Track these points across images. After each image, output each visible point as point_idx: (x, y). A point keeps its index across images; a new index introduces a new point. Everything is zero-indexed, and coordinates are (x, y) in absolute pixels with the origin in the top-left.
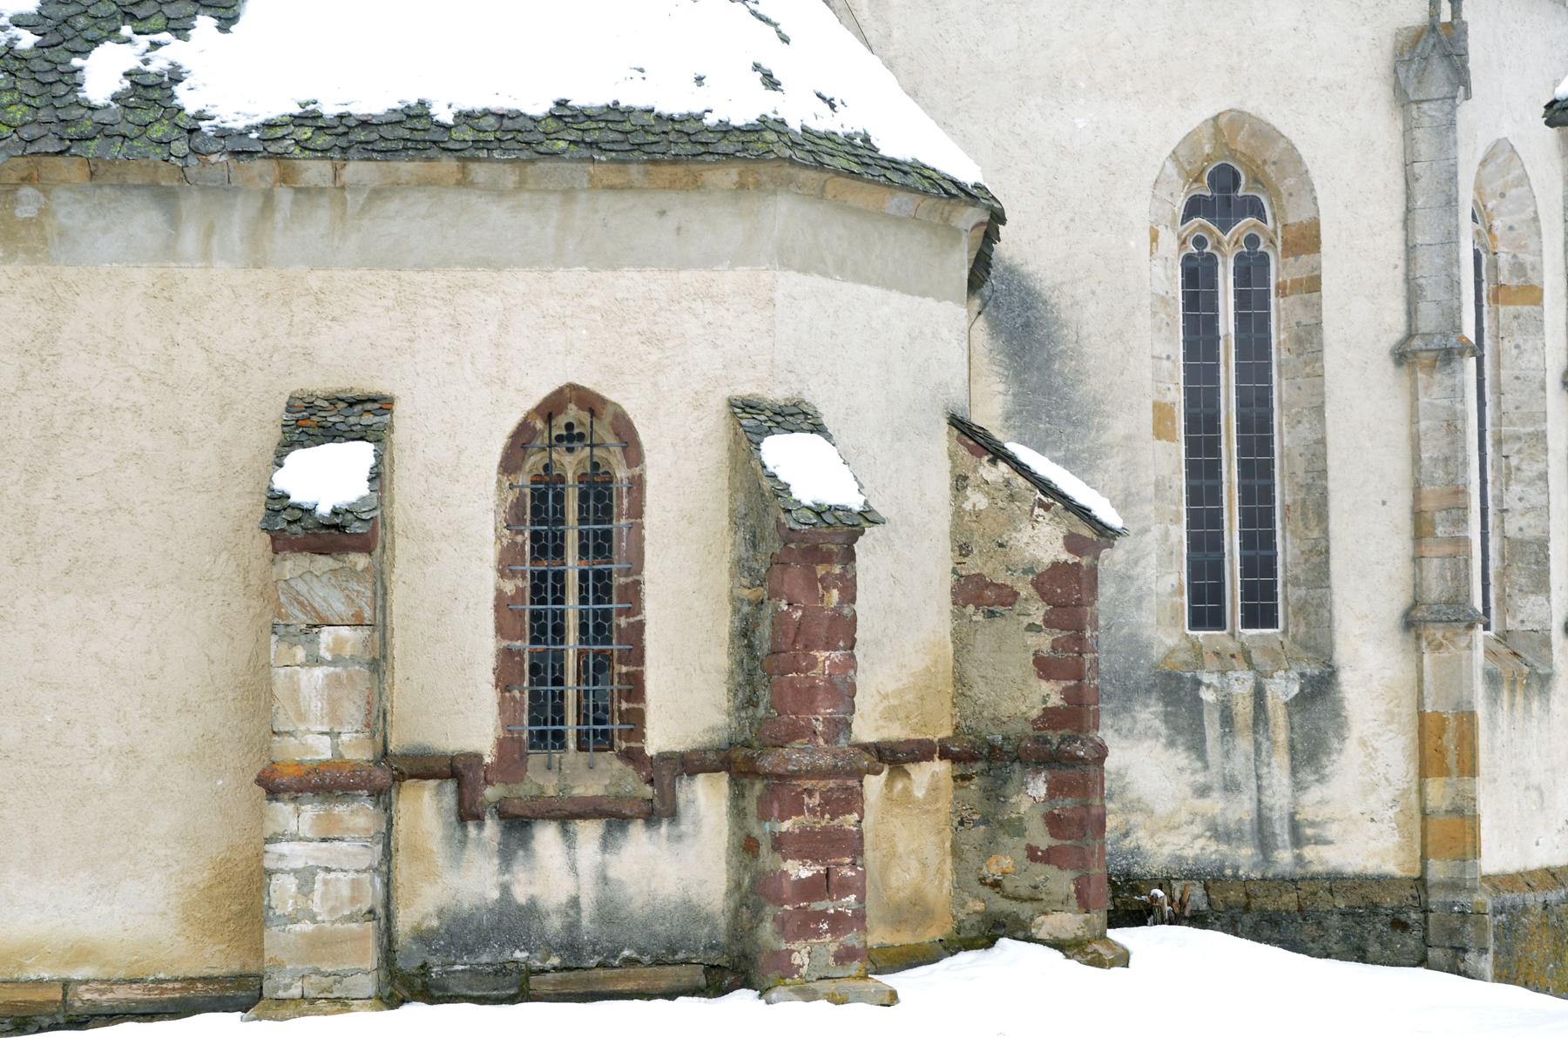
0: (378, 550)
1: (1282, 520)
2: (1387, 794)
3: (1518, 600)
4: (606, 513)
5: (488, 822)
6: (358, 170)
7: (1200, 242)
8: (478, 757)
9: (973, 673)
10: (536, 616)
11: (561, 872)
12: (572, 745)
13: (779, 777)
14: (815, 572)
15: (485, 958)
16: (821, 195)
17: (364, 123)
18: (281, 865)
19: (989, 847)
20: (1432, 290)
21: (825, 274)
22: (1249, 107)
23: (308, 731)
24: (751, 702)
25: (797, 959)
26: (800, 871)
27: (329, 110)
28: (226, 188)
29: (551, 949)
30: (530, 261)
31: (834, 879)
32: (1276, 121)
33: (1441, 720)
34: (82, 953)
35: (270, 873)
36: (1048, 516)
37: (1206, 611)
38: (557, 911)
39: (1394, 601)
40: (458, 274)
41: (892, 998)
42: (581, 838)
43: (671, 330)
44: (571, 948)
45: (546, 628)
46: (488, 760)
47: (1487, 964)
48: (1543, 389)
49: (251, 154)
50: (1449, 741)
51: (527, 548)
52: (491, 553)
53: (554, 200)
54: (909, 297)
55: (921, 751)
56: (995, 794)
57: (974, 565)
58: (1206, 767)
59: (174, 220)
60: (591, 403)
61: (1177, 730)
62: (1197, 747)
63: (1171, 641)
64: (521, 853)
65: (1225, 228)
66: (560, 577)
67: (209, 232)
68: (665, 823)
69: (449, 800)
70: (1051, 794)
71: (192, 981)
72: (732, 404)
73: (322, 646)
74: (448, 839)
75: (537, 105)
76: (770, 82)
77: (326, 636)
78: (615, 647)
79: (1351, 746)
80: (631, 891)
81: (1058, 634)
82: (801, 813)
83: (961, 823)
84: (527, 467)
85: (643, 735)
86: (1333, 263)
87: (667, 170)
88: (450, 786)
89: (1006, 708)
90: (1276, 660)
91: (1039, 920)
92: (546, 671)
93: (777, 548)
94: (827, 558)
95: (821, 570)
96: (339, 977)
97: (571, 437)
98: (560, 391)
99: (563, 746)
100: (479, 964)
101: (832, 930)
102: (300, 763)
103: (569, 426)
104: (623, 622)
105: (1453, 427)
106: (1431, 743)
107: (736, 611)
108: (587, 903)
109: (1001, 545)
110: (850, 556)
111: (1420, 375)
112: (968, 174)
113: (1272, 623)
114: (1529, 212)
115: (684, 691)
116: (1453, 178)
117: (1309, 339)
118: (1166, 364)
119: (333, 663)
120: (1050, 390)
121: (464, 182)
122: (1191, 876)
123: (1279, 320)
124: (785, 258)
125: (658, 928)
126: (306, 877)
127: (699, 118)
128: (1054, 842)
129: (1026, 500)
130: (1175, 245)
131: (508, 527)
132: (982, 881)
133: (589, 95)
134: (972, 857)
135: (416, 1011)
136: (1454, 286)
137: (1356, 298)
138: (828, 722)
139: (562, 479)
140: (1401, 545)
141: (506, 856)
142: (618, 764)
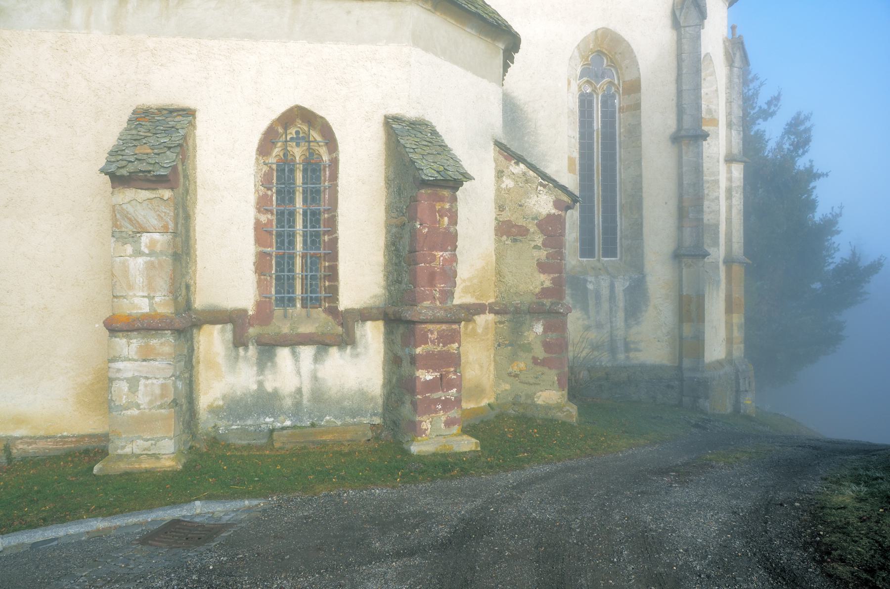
0: (181, 189)
1: (620, 211)
5: (251, 347)
8: (245, 311)
10: (279, 235)
12: (299, 305)
14: (434, 206)
15: (249, 422)
18: (118, 375)
19: (513, 358)
21: (436, 54)
22: (611, 27)
23: (135, 295)
31: (444, 380)
34: (19, 421)
35: (111, 380)
36: (545, 191)
37: (587, 249)
38: (290, 395)
45: (285, 240)
46: (251, 313)
48: (718, 162)
51: (274, 198)
52: (252, 199)
54: (476, 77)
55: (479, 309)
57: (506, 216)
58: (589, 318)
62: (585, 309)
63: (574, 262)
64: (269, 364)
68: (349, 348)
69: (229, 335)
70: (545, 331)
72: (386, 117)
73: (143, 245)
77: (145, 238)
78: (322, 251)
82: (426, 343)
83: (499, 345)
84: (274, 154)
85: (338, 300)
88: (229, 327)
91: (538, 394)
92: (285, 262)
98: (291, 110)
99: (294, 306)
100: (246, 425)
101: (443, 409)
102: (130, 315)
104: (326, 238)
108: (306, 390)
109: (520, 206)
110: (454, 199)
111: (683, 147)
113: (614, 255)
114: (714, 88)
118: (573, 140)
119: (147, 255)
123: (620, 123)
125: (345, 403)
126: (133, 383)
128: (547, 355)
129: (534, 182)
130: (577, 89)
131: (262, 185)
138: (442, 292)
139: (293, 160)
142: (323, 315)
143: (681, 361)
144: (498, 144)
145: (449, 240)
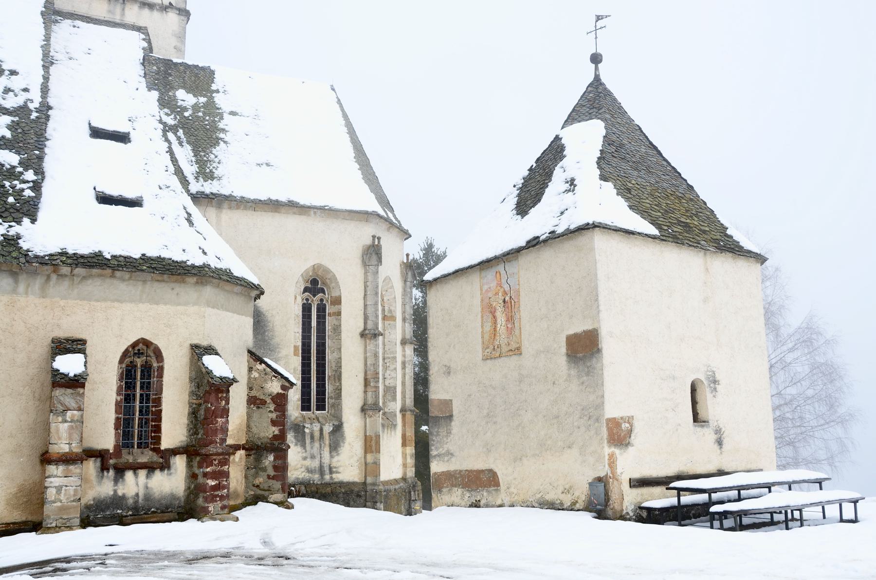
2: (356, 458)
3: (388, 403)
4: (149, 377)
6: (79, 271)
7: (307, 300)
8: (108, 450)
9: (252, 425)
11: (133, 485)
13: (207, 455)
16: (218, 286)
17: (82, 257)
19: (256, 475)
20: (371, 318)
22: (323, 263)
24: (196, 433)
25: (210, 509)
26: (212, 483)
27: (71, 251)
28: (35, 273)
29: (129, 509)
30: (131, 301)
32: (330, 267)
33: (371, 437)
35: (46, 488)
37: (305, 405)
39: (359, 404)
40: (109, 303)
41: (237, 519)
42: (140, 475)
43: (175, 324)
44: (136, 508)
47: (382, 506)
49: (46, 264)
50: (373, 443)
52: (115, 388)
53: (140, 283)
56: (258, 460)
59: (16, 282)
60: (146, 343)
61: (298, 441)
62: (304, 446)
65: (314, 296)
66: (134, 395)
67: (28, 286)
69: (98, 464)
70: (275, 460)
71: (9, 524)
74: (98, 476)
75: (137, 255)
76: (205, 253)
77: (69, 413)
79: (346, 445)
80: (155, 491)
81: (278, 413)
86: (345, 308)
87: (175, 277)
88: (99, 460)
89: (262, 435)
90: (326, 420)
93: (208, 389)
94: (222, 392)
95: (220, 395)
96: (69, 519)
97: (139, 354)
103: (139, 350)
105: (376, 355)
106: (368, 444)
107: (190, 406)
110: (228, 391)
112: (256, 281)
115: (174, 430)
116: (377, 287)
117: (337, 329)
119: (70, 422)
120: (264, 341)
121: (113, 276)
122: (301, 483)
124: (209, 304)
125: (163, 502)
126: (59, 489)
127: (185, 262)
132: (254, 485)
133: (152, 253)
134: (251, 478)
135: (91, 530)
136: (377, 316)
137: (350, 320)
139: (136, 366)
140: (361, 388)
141: (116, 481)
142: (151, 452)
143: (366, 479)
144: (249, 352)
145: (225, 412)
